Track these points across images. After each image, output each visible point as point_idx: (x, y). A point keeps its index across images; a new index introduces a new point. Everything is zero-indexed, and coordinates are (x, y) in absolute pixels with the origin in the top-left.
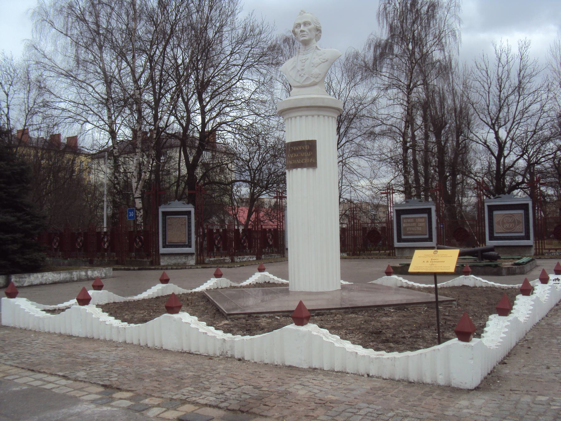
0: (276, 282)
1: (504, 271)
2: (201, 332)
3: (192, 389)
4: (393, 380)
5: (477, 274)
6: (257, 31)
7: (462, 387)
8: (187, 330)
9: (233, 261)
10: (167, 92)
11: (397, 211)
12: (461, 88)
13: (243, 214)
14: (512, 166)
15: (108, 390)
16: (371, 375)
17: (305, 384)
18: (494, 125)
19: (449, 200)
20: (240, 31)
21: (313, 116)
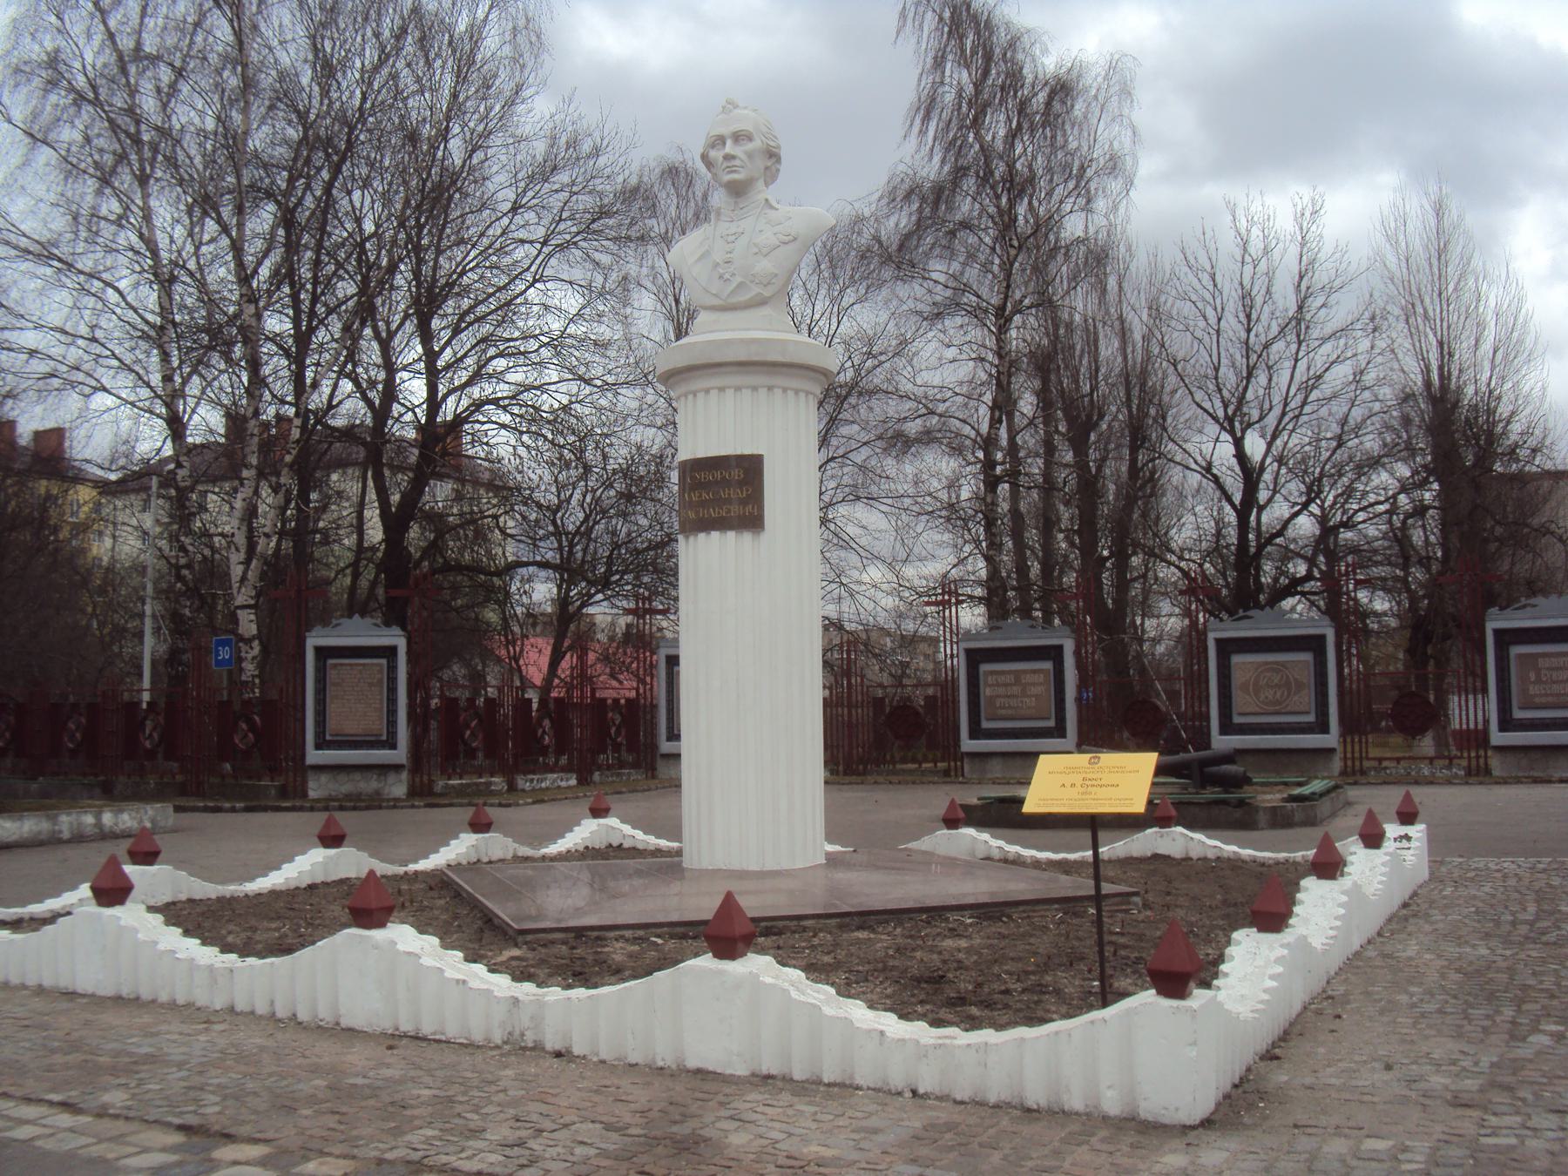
0: (640, 846)
1: (1262, 818)
2: (449, 980)
3: (436, 1133)
4: (981, 1104)
5: (1191, 826)
6: (586, 147)
7: (1166, 1121)
8: (407, 973)
9: (512, 788)
10: (330, 312)
11: (968, 652)
12: (1145, 317)
13: (536, 659)
14: (1280, 533)
15: (195, 1139)
16: (921, 1091)
17: (744, 1116)
18: (1233, 423)
19: (1110, 624)
20: (540, 148)
21: (755, 389)
